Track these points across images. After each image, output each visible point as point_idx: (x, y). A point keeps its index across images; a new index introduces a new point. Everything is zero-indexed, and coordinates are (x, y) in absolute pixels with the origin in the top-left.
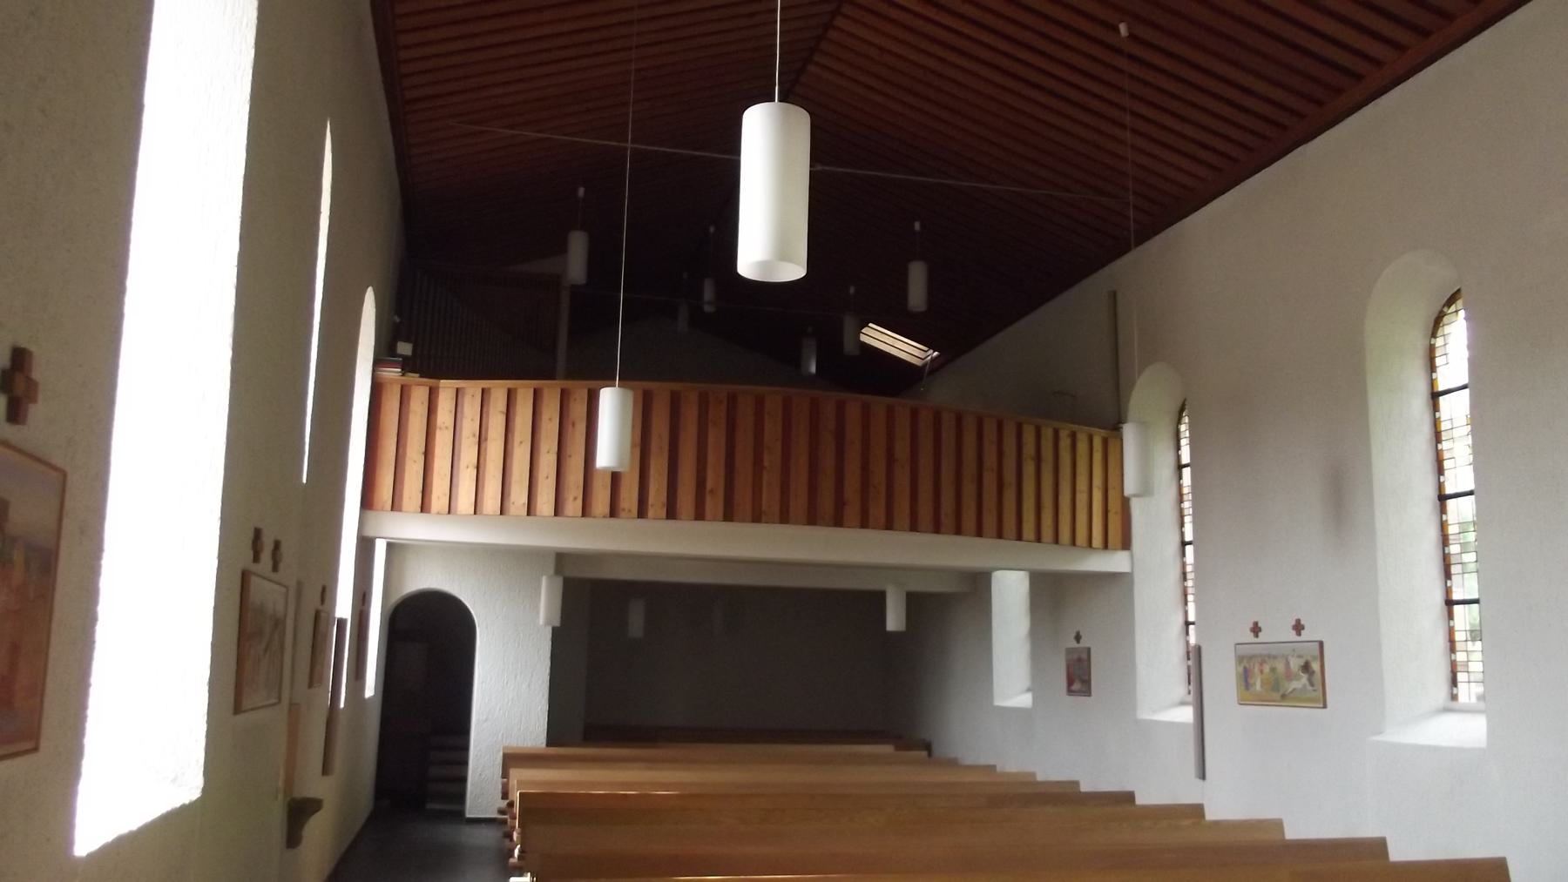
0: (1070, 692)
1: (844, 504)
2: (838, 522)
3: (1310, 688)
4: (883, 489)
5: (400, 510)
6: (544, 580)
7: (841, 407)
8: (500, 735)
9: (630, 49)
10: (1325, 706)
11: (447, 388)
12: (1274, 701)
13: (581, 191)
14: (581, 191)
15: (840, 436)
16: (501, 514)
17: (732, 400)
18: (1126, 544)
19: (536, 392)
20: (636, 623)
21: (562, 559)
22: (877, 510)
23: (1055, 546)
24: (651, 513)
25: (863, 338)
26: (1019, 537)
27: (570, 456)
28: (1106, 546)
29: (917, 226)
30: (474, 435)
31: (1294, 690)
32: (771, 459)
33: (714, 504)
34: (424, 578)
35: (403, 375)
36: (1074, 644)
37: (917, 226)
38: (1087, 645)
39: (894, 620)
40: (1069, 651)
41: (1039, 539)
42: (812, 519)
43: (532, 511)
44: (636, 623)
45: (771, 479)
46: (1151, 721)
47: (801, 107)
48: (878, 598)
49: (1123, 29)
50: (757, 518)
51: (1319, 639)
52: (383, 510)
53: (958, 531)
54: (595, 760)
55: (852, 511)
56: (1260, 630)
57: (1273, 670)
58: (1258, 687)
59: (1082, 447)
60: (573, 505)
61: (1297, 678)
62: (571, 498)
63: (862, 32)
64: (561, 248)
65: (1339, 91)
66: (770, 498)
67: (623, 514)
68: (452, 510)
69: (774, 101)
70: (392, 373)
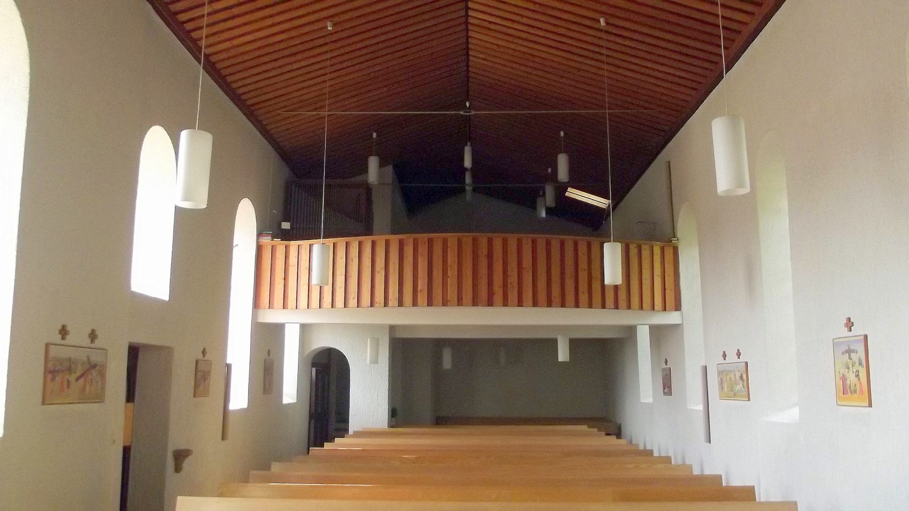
0: (665, 394)
1: (494, 294)
2: (490, 303)
3: (743, 389)
4: (516, 284)
5: (273, 308)
6: (369, 340)
7: (490, 241)
8: (364, 422)
9: (326, 74)
10: (749, 400)
11: (294, 244)
12: (732, 397)
13: (375, 135)
14: (375, 135)
15: (490, 256)
16: (320, 308)
17: (430, 241)
18: (678, 307)
19: (347, 243)
20: (447, 361)
21: (392, 328)
22: (513, 296)
23: (641, 311)
24: (390, 304)
25: (567, 194)
26: (604, 307)
27: (351, 276)
28: (665, 309)
29: (562, 134)
30: (307, 268)
31: (738, 390)
32: (452, 273)
33: (422, 297)
34: (322, 341)
35: (272, 240)
36: (665, 366)
37: (562, 134)
38: (670, 367)
39: (563, 355)
40: (664, 370)
41: (641, 308)
42: (475, 303)
43: (347, 305)
44: (447, 361)
45: (452, 282)
46: (692, 409)
47: (209, 132)
48: (554, 342)
49: (602, 21)
50: (445, 303)
51: (745, 361)
52: (265, 308)
53: (563, 305)
54: (423, 434)
55: (498, 297)
56: (723, 356)
57: (730, 379)
58: (726, 389)
59: (646, 253)
60: (353, 302)
61: (737, 384)
62: (352, 299)
63: (486, 38)
64: (365, 170)
65: (733, 41)
66: (452, 293)
67: (377, 305)
68: (321, 307)
69: (195, 129)
70: (267, 240)
